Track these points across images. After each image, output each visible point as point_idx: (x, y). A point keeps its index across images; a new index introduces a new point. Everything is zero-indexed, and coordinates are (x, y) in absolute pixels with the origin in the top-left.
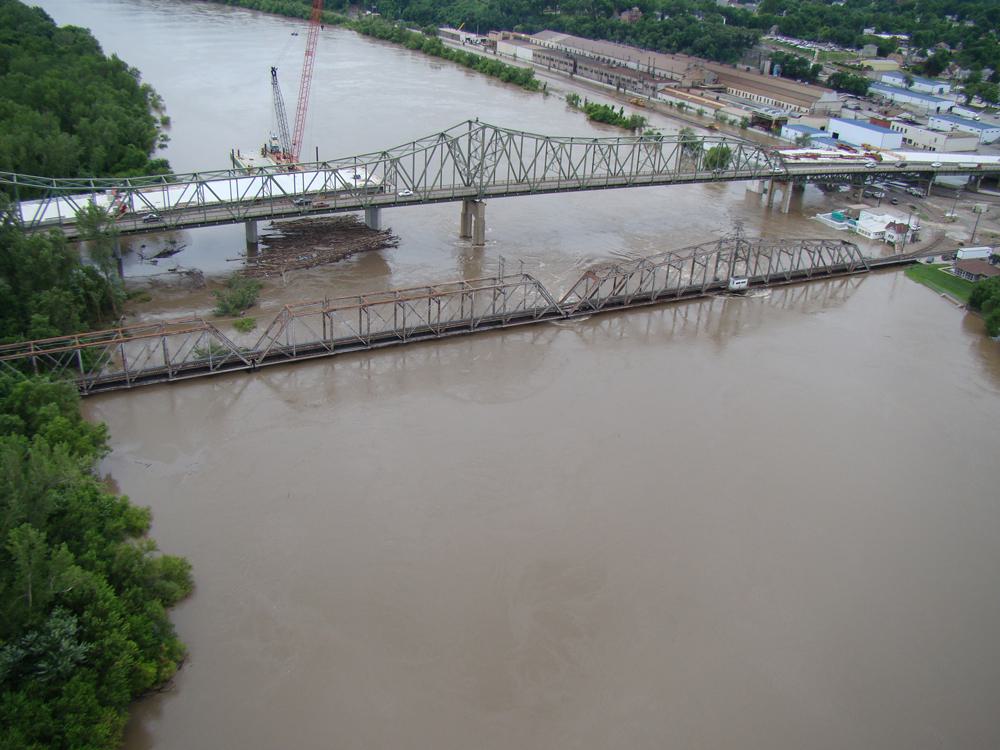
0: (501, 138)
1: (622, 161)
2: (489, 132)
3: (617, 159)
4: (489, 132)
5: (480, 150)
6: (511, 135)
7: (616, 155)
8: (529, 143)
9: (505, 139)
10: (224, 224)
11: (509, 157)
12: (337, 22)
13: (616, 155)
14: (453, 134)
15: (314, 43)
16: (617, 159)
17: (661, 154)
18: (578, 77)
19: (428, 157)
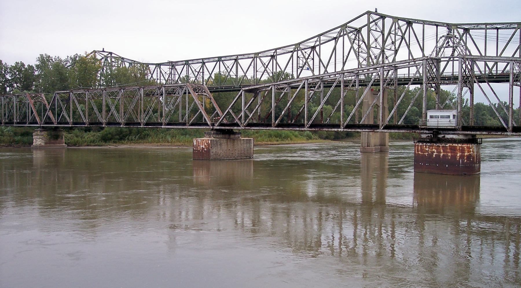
0: (399, 28)
1: (325, 61)
2: (388, 22)
3: (320, 60)
4: (388, 22)
5: (380, 40)
6: (409, 23)
7: (319, 56)
8: (430, 30)
9: (403, 29)
10: (236, 70)
11: (409, 46)
12: (485, 177)
13: (319, 56)
14: (356, 24)
15: (215, 130)
16: (320, 60)
17: (277, 63)
18: (278, 217)
19: (408, 41)
